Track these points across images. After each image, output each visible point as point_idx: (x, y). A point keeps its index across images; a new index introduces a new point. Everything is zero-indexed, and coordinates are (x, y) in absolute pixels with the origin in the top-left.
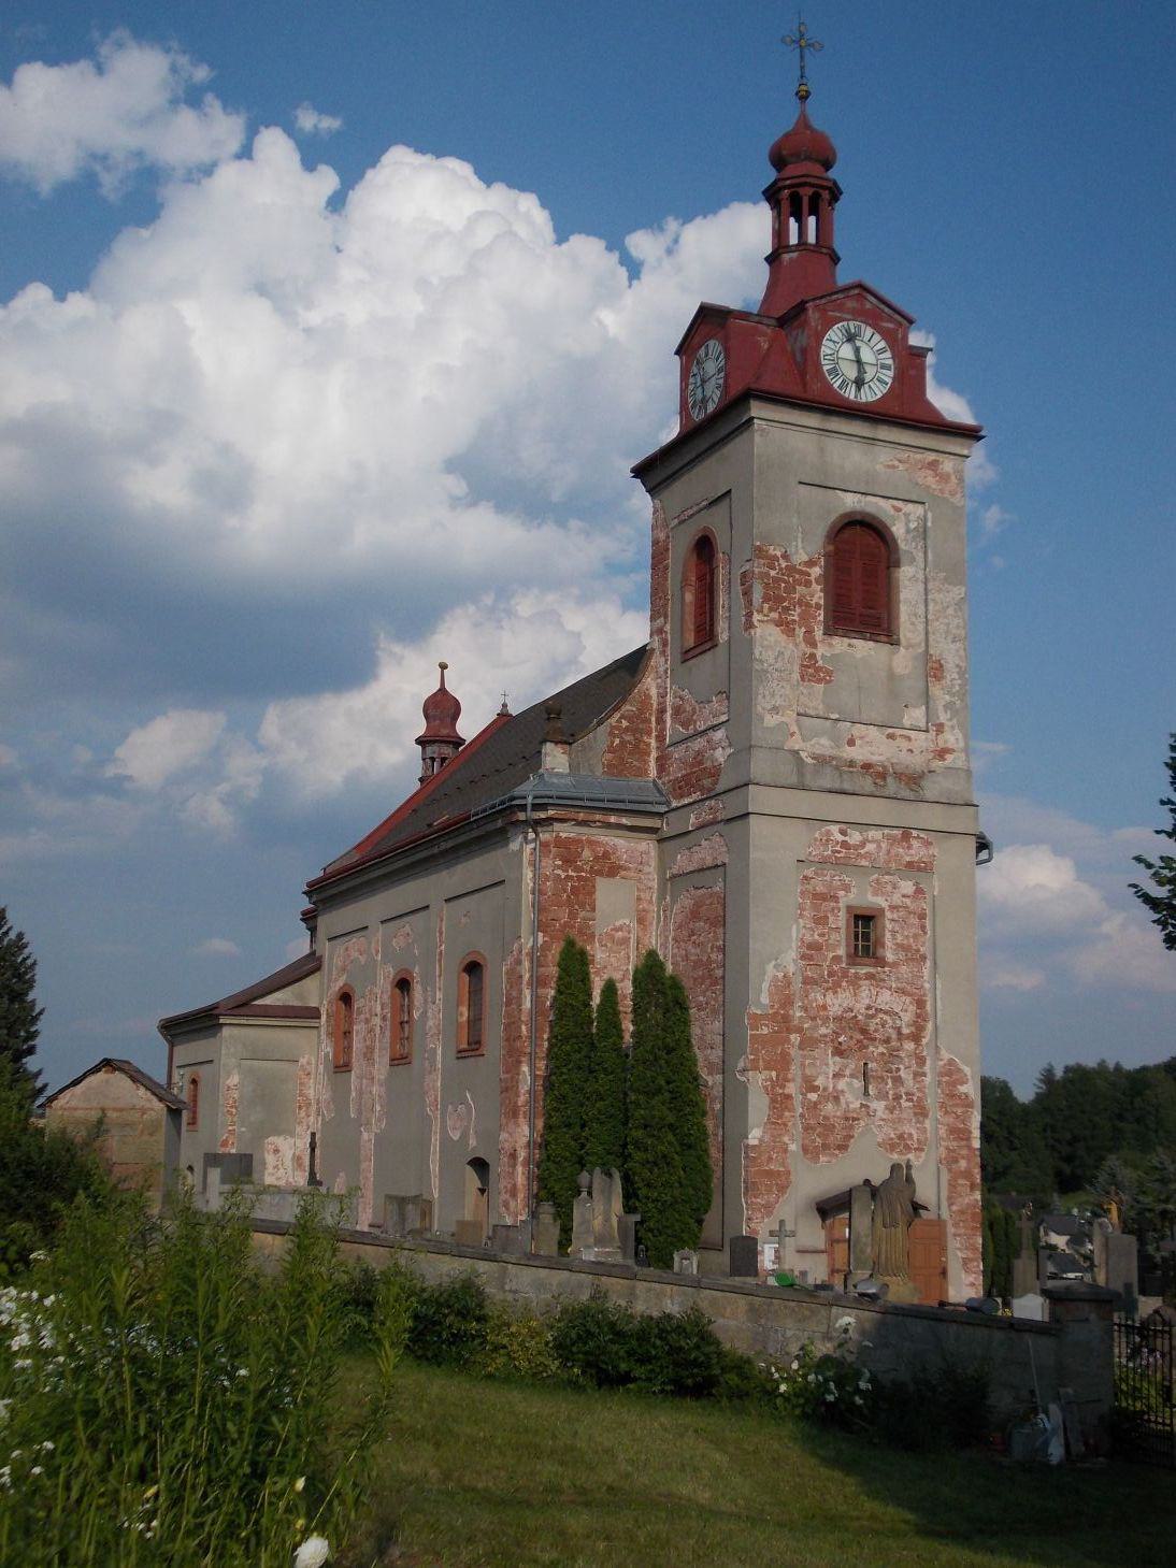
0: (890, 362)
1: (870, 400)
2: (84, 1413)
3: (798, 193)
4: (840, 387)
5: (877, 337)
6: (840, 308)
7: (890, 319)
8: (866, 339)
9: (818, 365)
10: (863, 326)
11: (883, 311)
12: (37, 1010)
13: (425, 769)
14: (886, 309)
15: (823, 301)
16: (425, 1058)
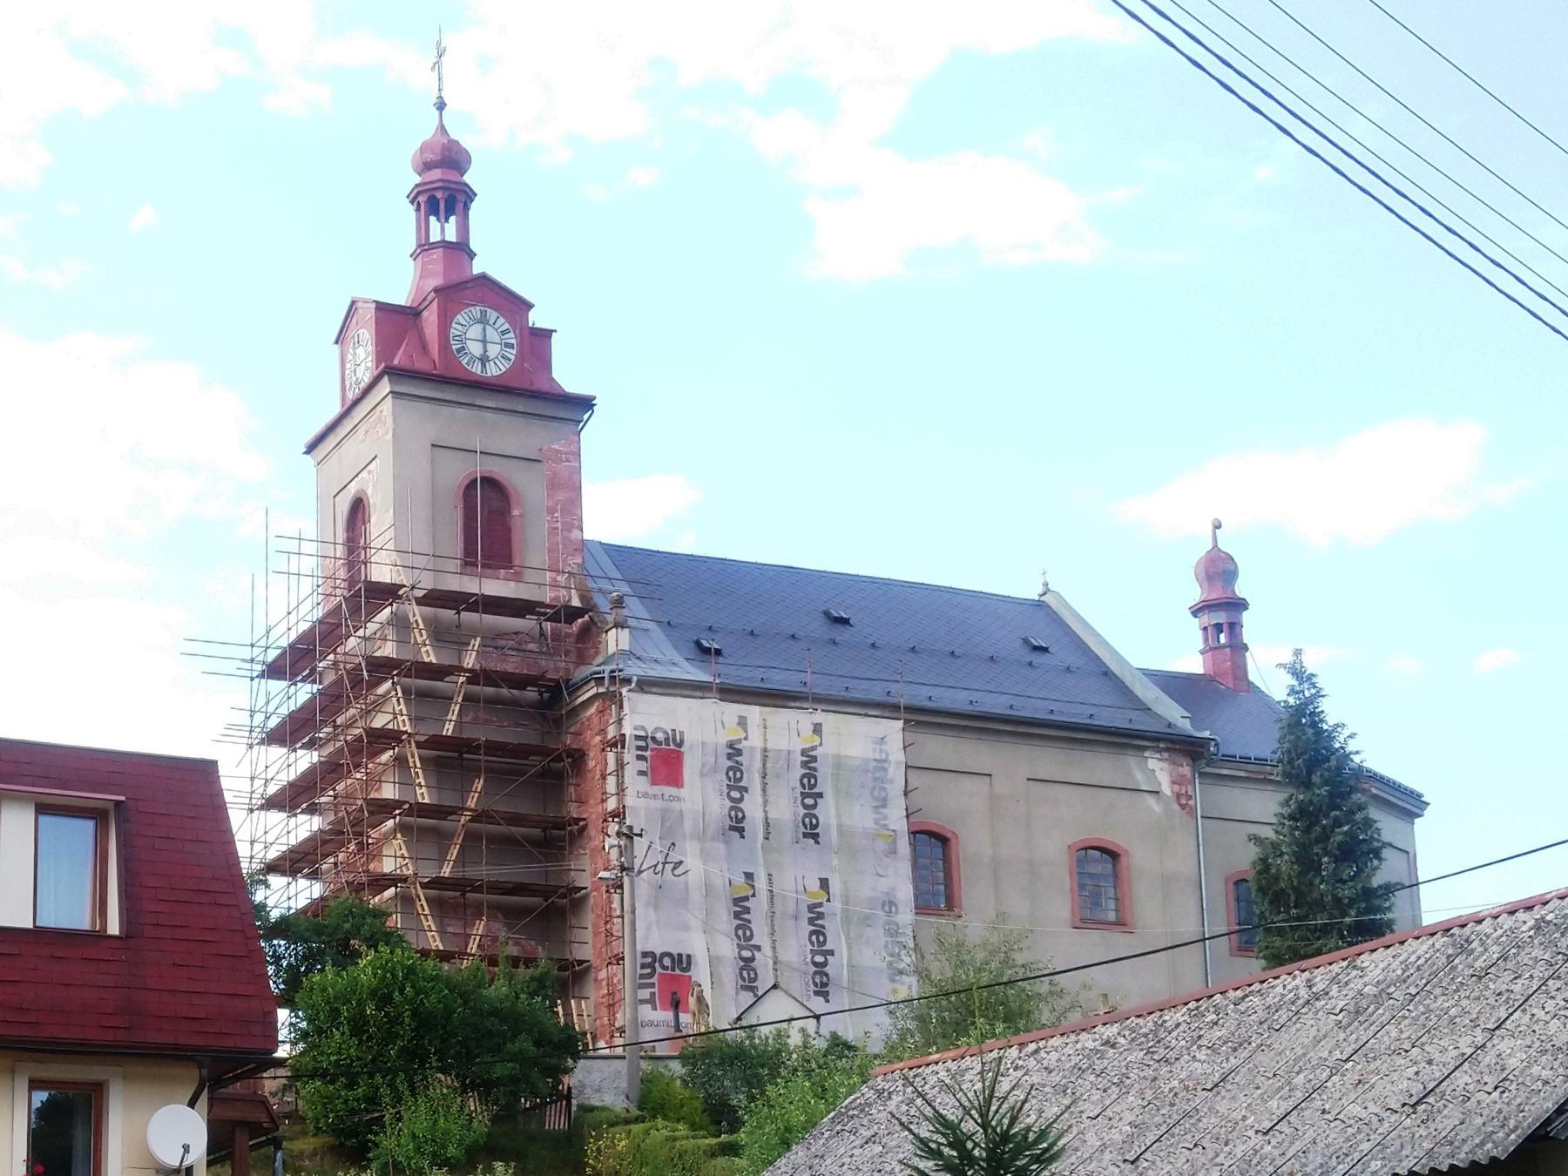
1: (495, 374)
3: (435, 197)
4: (468, 364)
8: (491, 322)
13: (1206, 640)
16: (1395, 985)
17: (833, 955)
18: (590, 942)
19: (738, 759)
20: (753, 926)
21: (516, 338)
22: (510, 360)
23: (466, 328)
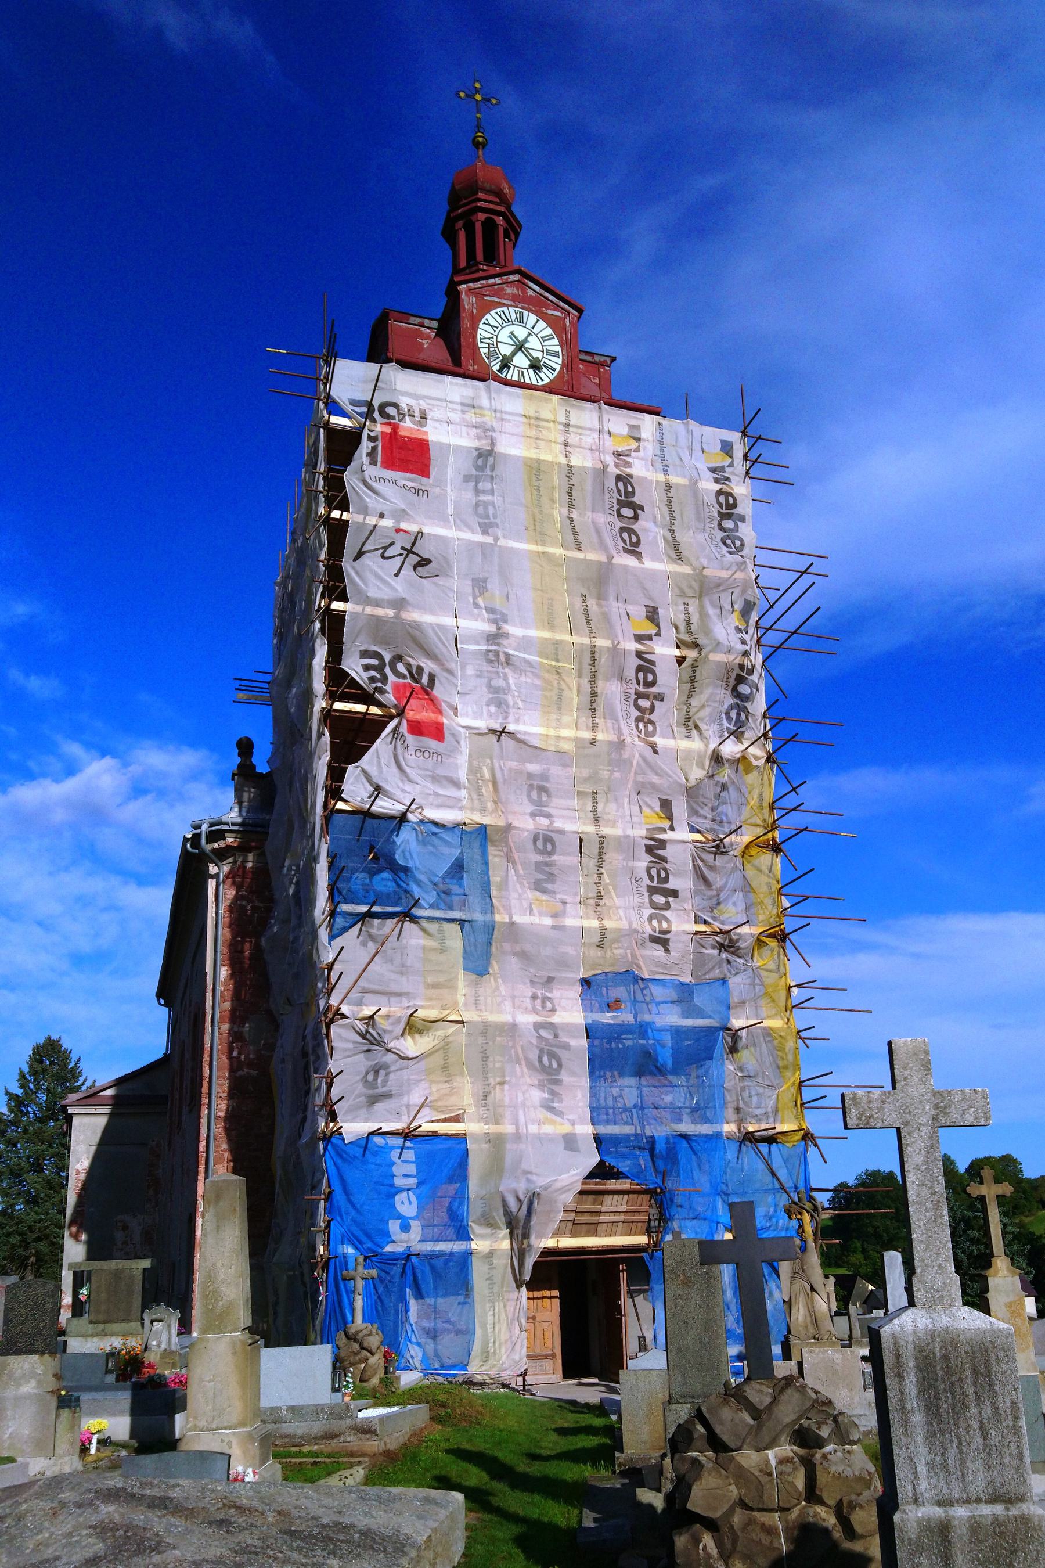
0: (558, 349)
2: (544, 777)
5: (542, 324)
6: (498, 293)
7: (557, 307)
9: (475, 349)
10: (526, 313)
11: (547, 298)
12: (549, 886)
14: (551, 297)
15: (478, 284)
17: (662, 700)
18: (392, 581)
19: (660, 852)
20: (657, 669)
21: (561, 345)
22: (554, 370)
23: (497, 330)
